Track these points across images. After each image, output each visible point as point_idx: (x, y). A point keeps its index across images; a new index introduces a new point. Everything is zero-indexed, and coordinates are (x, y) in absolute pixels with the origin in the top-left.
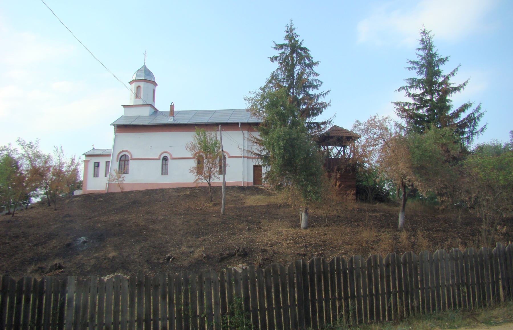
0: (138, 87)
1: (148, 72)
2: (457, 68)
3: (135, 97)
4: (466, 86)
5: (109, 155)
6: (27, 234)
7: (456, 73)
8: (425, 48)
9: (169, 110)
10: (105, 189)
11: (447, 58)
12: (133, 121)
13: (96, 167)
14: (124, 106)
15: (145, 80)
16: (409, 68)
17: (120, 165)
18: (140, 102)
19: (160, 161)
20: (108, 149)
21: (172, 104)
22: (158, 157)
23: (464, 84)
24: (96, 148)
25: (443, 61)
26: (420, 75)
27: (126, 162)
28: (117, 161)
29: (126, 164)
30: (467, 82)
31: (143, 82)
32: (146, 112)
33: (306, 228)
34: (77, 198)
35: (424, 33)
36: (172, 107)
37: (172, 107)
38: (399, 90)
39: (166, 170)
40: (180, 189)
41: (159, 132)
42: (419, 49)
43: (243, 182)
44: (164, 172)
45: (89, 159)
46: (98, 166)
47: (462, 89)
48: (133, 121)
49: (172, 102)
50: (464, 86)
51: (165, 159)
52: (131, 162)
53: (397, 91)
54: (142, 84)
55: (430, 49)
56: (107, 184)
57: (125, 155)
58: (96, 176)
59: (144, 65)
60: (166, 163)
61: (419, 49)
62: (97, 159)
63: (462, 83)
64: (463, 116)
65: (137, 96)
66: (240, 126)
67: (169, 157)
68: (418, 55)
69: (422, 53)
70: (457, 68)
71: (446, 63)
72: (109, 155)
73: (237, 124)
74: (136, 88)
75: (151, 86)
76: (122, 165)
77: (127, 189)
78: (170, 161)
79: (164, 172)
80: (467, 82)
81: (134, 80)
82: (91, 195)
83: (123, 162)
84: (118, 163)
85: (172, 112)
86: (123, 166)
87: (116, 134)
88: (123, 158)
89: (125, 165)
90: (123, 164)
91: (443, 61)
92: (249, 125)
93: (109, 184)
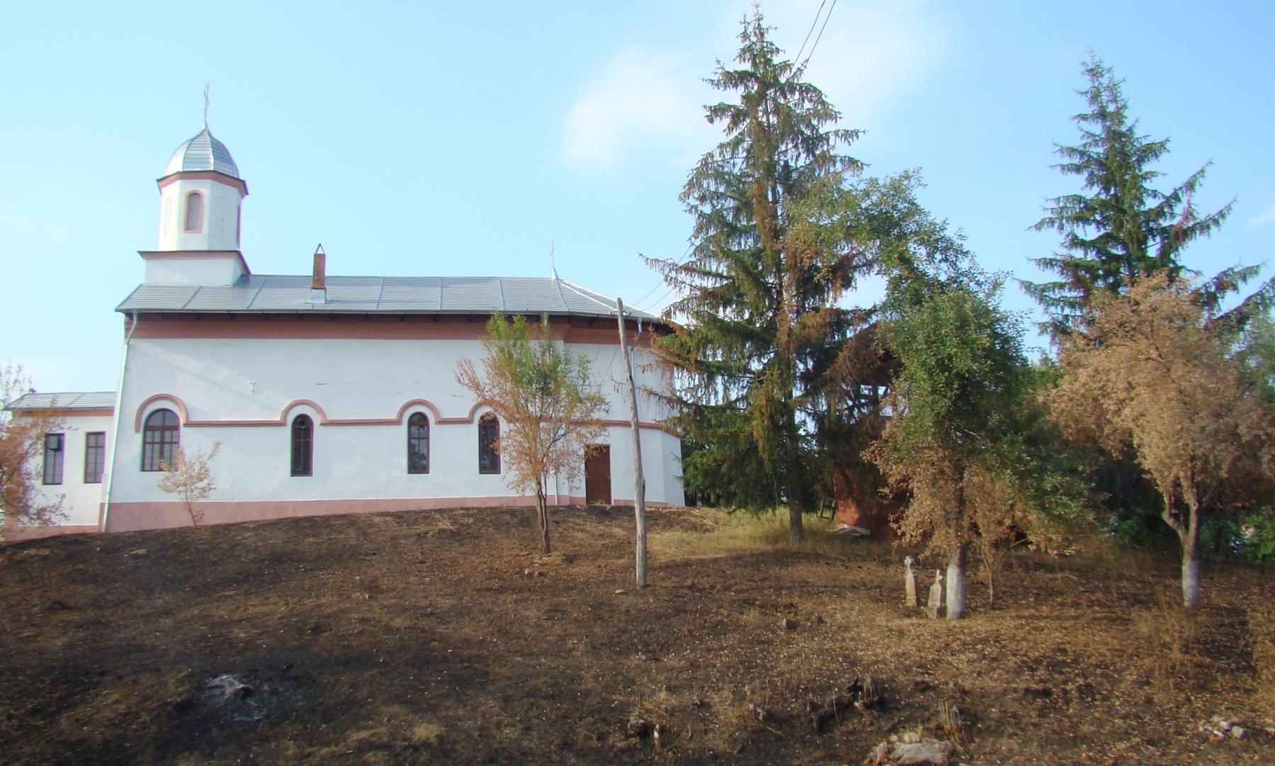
0: (193, 198)
1: (220, 151)
2: (1202, 171)
3: (182, 228)
4: (1226, 221)
5: (108, 411)
6: (439, 608)
7: (1201, 185)
8: (1102, 115)
9: (312, 274)
10: (96, 523)
11: (1162, 145)
12: (189, 301)
13: (52, 453)
14: (144, 254)
15: (217, 176)
16: (1063, 167)
17: (145, 443)
18: (198, 242)
19: (402, 431)
20: (84, 394)
21: (320, 252)
22: (278, 418)
23: (1222, 214)
24: (38, 391)
25: (1151, 151)
26: (1088, 189)
27: (168, 434)
28: (137, 431)
29: (167, 439)
30: (1229, 208)
31: (210, 181)
32: (225, 272)
33: (962, 615)
34: (33, 551)
35: (1094, 72)
36: (319, 260)
37: (319, 260)
38: (1039, 226)
39: (57, 467)
40: (406, 515)
41: (354, 338)
42: (1084, 117)
43: (558, 496)
44: (302, 462)
45: (27, 421)
46: (59, 448)
47: (1213, 229)
48: (189, 301)
49: (320, 245)
50: (1221, 221)
51: (419, 423)
52: (186, 435)
53: (1033, 229)
54: (206, 188)
55: (1118, 116)
56: (102, 505)
57: (164, 410)
58: (49, 479)
59: (203, 128)
60: (174, 440)
61: (1084, 117)
62: (95, 424)
63: (1213, 212)
64: (1229, 302)
65: (191, 221)
66: (640, 330)
67: (316, 419)
68: (1082, 133)
69: (1097, 128)
70: (1202, 171)
71: (1164, 157)
72: (108, 411)
73: (610, 322)
74: (184, 198)
75: (233, 192)
76: (153, 443)
77: (211, 519)
78: (435, 430)
79: (302, 462)
80: (1229, 208)
81: (178, 173)
82: (80, 538)
83: (158, 434)
84: (140, 437)
85: (319, 280)
86: (157, 447)
87: (133, 341)
88: (157, 421)
89: (162, 443)
90: (158, 440)
91: (1151, 151)
92: (569, 322)
93: (110, 504)
